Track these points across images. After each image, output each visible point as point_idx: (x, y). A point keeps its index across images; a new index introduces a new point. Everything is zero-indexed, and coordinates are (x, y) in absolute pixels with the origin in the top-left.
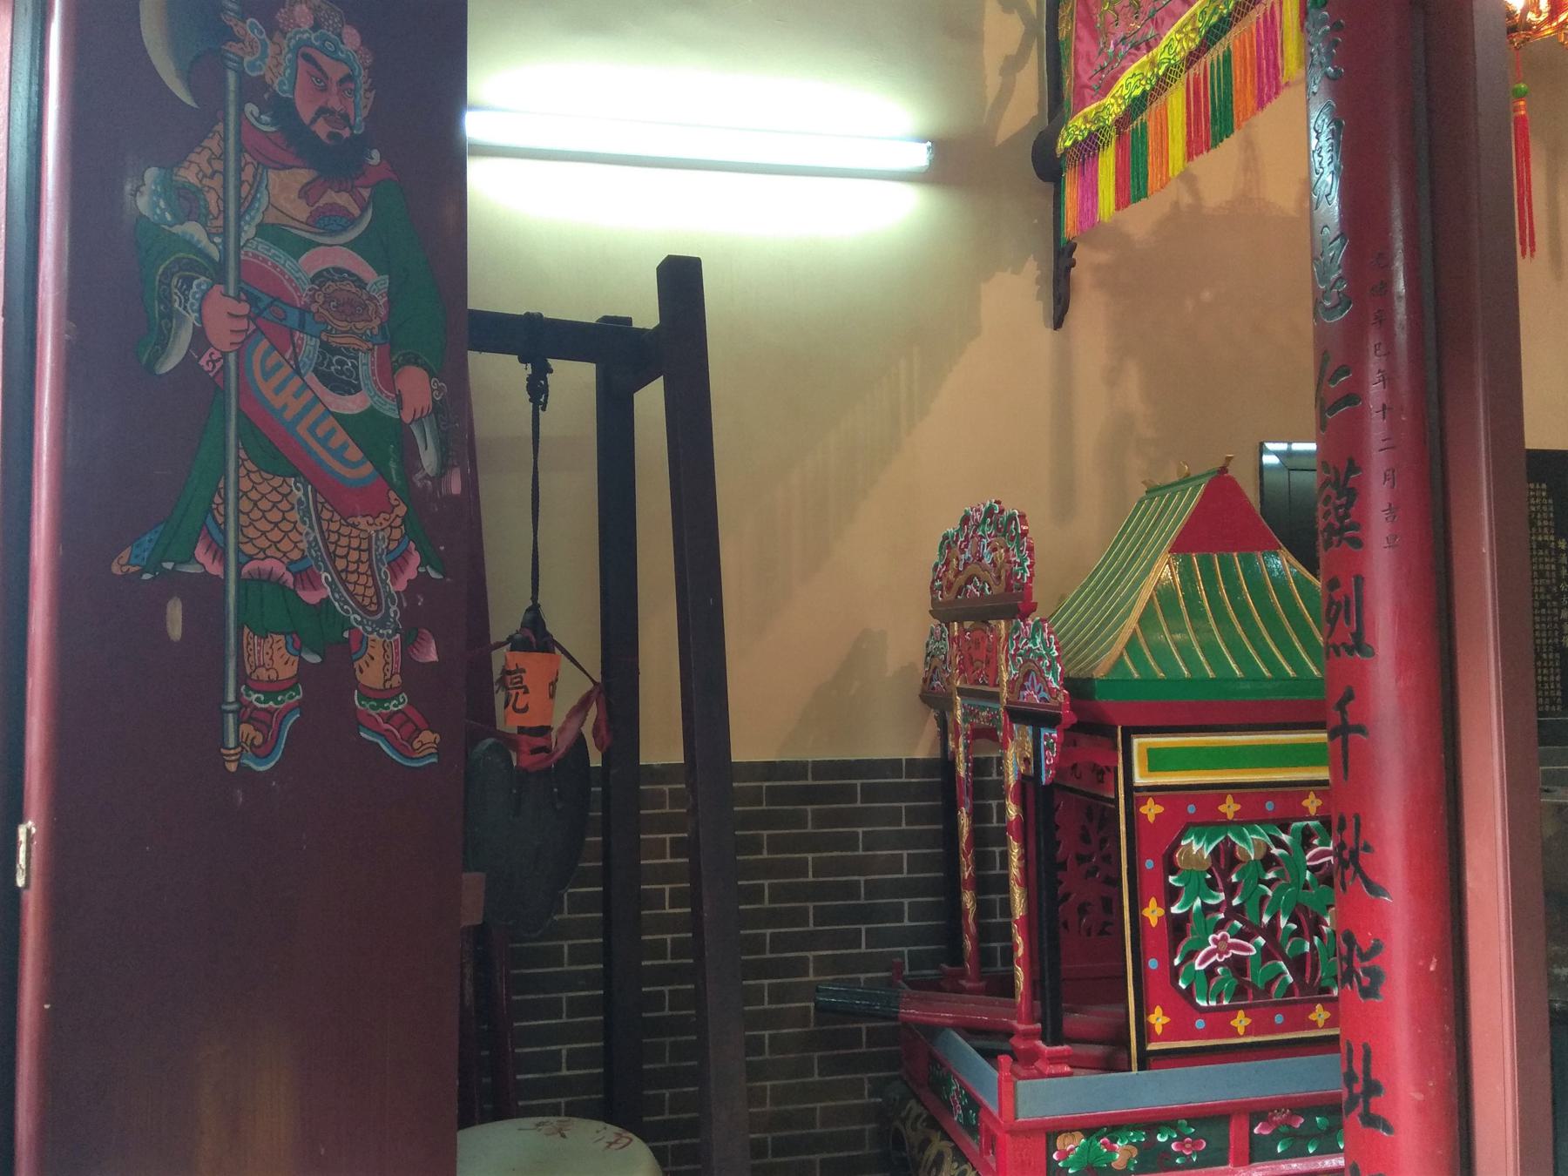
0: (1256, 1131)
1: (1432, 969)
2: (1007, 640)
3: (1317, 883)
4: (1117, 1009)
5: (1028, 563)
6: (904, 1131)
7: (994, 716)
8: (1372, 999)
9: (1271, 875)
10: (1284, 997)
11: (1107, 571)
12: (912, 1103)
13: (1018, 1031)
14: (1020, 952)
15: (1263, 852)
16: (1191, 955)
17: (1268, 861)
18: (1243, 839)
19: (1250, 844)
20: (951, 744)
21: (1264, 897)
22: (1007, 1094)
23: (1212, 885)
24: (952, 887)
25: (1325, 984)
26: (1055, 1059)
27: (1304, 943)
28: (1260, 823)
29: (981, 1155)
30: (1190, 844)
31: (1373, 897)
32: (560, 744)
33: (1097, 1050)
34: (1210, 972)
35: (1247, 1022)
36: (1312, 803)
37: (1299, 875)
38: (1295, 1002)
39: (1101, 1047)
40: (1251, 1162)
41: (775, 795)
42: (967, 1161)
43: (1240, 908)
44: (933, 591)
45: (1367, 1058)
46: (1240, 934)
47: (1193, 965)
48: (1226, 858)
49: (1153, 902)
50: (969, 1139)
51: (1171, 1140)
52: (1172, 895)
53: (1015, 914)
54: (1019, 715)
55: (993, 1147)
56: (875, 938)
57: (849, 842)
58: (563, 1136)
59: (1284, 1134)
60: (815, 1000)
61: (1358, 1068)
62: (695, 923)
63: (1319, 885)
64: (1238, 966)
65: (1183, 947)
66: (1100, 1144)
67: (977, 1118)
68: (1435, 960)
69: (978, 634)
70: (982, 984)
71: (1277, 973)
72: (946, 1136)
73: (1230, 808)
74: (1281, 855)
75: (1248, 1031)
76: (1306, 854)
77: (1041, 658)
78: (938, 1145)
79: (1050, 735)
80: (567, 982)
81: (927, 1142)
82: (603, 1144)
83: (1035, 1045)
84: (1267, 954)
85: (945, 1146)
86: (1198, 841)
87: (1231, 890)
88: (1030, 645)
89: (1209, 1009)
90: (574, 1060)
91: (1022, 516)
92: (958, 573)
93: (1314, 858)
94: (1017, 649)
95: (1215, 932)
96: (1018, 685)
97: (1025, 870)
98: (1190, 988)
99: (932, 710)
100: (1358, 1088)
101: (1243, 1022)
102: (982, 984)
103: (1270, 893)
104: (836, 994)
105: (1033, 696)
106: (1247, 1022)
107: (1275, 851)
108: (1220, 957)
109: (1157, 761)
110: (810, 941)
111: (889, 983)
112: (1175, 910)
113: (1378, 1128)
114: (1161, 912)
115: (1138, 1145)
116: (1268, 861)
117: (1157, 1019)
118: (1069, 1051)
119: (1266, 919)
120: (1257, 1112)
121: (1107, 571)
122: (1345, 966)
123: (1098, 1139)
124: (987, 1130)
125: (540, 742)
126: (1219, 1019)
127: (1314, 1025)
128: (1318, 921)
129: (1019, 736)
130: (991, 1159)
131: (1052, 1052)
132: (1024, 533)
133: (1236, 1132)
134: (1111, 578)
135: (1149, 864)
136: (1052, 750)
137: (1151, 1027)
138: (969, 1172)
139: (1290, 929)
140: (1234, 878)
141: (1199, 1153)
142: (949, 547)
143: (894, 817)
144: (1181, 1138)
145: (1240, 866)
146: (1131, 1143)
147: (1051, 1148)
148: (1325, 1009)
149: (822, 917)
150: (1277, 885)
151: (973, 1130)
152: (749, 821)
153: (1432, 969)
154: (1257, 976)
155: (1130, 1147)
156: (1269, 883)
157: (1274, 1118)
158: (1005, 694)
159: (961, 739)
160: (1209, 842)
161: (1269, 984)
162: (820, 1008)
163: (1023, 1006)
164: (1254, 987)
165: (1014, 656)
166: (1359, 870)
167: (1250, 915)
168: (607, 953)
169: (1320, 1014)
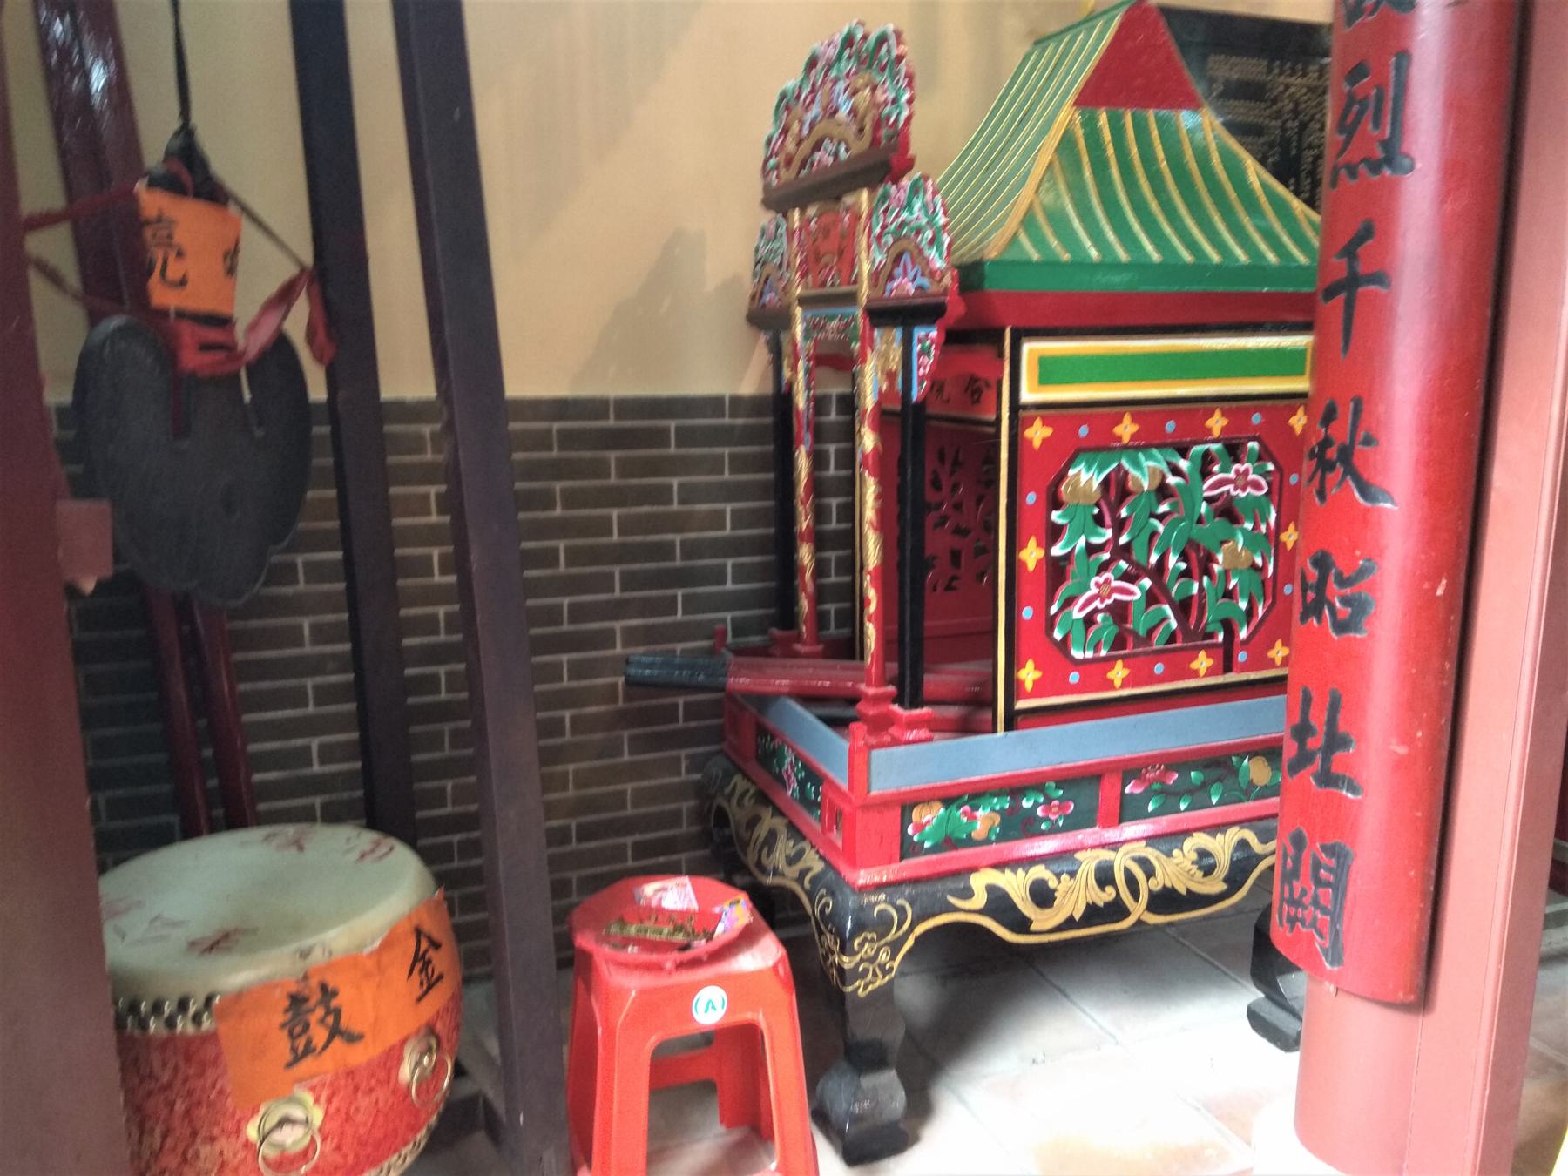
0: (1128, 790)
1: (1440, 592)
2: (870, 216)
3: (1212, 515)
4: (976, 667)
5: (906, 96)
6: (727, 809)
7: (847, 325)
8: (1352, 635)
9: (1164, 508)
10: (1166, 644)
11: (984, 144)
12: (738, 778)
13: (866, 695)
14: (872, 607)
15: (1157, 483)
16: (1069, 602)
17: (1163, 492)
18: (1137, 465)
19: (1144, 471)
20: (787, 373)
21: (1154, 534)
22: (859, 767)
23: (1099, 520)
24: (785, 543)
25: (1210, 629)
26: (913, 724)
27: (1192, 584)
28: (1159, 447)
29: (824, 831)
30: (1079, 473)
31: (1368, 505)
32: (249, 340)
33: (952, 712)
34: (1089, 621)
35: (1125, 673)
36: (1217, 423)
37: (1194, 506)
38: (1181, 649)
39: (957, 708)
40: (1121, 821)
41: (569, 439)
42: (804, 838)
43: (1128, 546)
44: (765, 173)
45: (1334, 708)
46: (1126, 577)
47: (1071, 613)
48: (1117, 489)
49: (1032, 543)
50: (805, 813)
51: (1036, 805)
52: (1055, 532)
53: (868, 566)
54: (886, 315)
55: (837, 824)
56: (692, 604)
57: (662, 495)
58: (301, 848)
59: (1155, 791)
60: (625, 674)
61: (1318, 719)
62: (464, 591)
63: (1215, 517)
64: (1120, 612)
65: (1062, 593)
66: (960, 814)
67: (817, 793)
68: (1444, 582)
69: (827, 219)
70: (820, 648)
71: (1161, 618)
72: (778, 812)
73: (1126, 429)
74: (1178, 485)
75: (1126, 683)
76: (1204, 483)
77: (918, 231)
78: (769, 821)
79: (928, 335)
80: (315, 666)
81: (754, 821)
82: (355, 855)
83: (889, 710)
84: (1151, 598)
85: (779, 823)
86: (1089, 469)
87: (1120, 526)
88: (905, 215)
89: (1085, 661)
90: (327, 755)
91: (898, 34)
92: (799, 143)
93: (1213, 487)
94: (884, 227)
95: (1098, 573)
96: (883, 275)
97: (881, 513)
98: (1065, 639)
99: (762, 334)
100: (1316, 742)
101: (1120, 673)
102: (820, 648)
103: (1161, 528)
104: (651, 666)
105: (905, 286)
106: (1125, 673)
107: (1172, 480)
108: (1102, 601)
109: (1050, 371)
110: (617, 610)
111: (712, 652)
112: (1058, 550)
113: (1342, 788)
114: (1040, 553)
115: (1002, 812)
116: (1163, 492)
117: (1028, 674)
118: (928, 714)
119: (1154, 558)
120: (1130, 769)
121: (984, 144)
122: (1311, 595)
123: (959, 808)
124: (832, 805)
125: (214, 335)
126: (1095, 671)
127: (1195, 674)
128: (1210, 558)
129: (882, 344)
130: (837, 838)
131: (910, 716)
132: (899, 59)
133: (1108, 792)
134: (991, 151)
135: (1031, 498)
136: (928, 354)
137: (1021, 683)
138: (807, 852)
139: (1178, 569)
140: (1124, 513)
141: (1066, 818)
142: (787, 107)
143: (715, 466)
144: (1048, 800)
145: (1131, 499)
146: (993, 810)
147: (905, 819)
148: (1208, 656)
149: (630, 582)
150: (1168, 519)
151: (811, 805)
152: (533, 471)
153: (1440, 592)
154: (1139, 622)
155: (993, 815)
156: (1161, 518)
157: (1148, 775)
158: (865, 291)
159: (801, 364)
160: (1100, 471)
161: (1151, 632)
162: (630, 683)
163: (873, 670)
164: (1134, 633)
165: (879, 237)
166: (1351, 471)
167: (1137, 555)
168: (355, 631)
169: (1203, 662)
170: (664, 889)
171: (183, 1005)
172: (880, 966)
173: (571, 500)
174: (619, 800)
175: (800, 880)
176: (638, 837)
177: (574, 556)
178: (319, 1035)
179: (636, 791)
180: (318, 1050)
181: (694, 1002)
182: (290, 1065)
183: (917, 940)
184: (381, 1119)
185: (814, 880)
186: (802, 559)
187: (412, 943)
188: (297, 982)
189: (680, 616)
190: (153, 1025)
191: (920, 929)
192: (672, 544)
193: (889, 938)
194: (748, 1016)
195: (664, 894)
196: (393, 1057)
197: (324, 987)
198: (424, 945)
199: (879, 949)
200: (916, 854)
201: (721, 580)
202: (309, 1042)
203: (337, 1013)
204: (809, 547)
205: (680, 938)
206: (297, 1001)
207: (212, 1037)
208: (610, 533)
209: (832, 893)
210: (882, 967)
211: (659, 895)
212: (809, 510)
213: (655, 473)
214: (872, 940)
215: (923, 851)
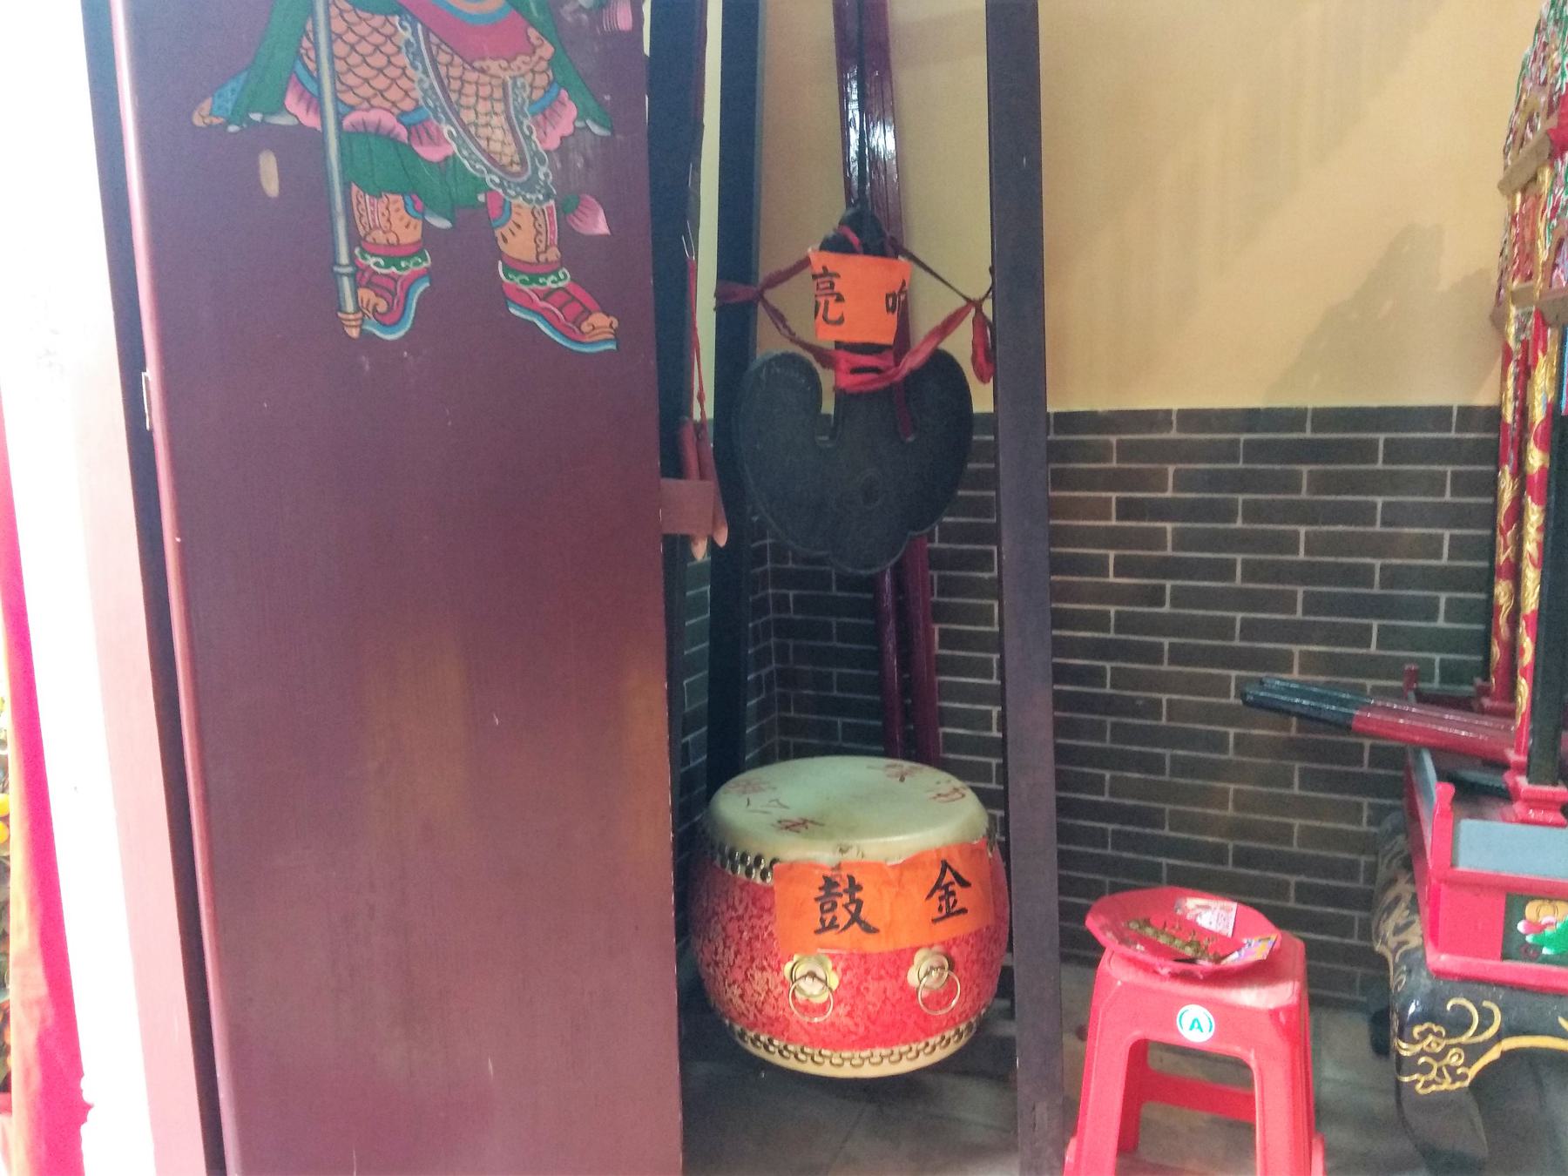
41: (1256, 451)
81: (1392, 882)
82: (933, 794)
110: (1298, 633)
143: (1435, 483)
149: (1314, 603)
170: (1207, 908)
171: (758, 860)
172: (1448, 1066)
173: (1253, 512)
174: (1284, 833)
175: (1394, 952)
176: (1303, 878)
177: (1252, 572)
178: (843, 917)
179: (1304, 829)
180: (840, 928)
181: (1179, 1015)
182: (818, 932)
183: (1504, 1054)
184: (888, 1007)
185: (1406, 954)
186: (1498, 598)
187: (937, 872)
188: (833, 869)
189: (1373, 649)
190: (740, 869)
191: (1510, 1043)
192: (1370, 569)
193: (1464, 1039)
194: (1237, 1050)
195: (1203, 911)
196: (902, 959)
197: (851, 879)
198: (949, 877)
199: (1447, 1048)
200: (1532, 959)
201: (1431, 615)
202: (835, 918)
203: (859, 903)
204: (1508, 585)
205: (1189, 951)
206: (829, 884)
207: (770, 890)
208: (1296, 552)
209: (1409, 972)
210: (1452, 1070)
211: (1198, 911)
212: (1509, 541)
213: (1354, 490)
214: (1438, 1035)
215: (1540, 958)
